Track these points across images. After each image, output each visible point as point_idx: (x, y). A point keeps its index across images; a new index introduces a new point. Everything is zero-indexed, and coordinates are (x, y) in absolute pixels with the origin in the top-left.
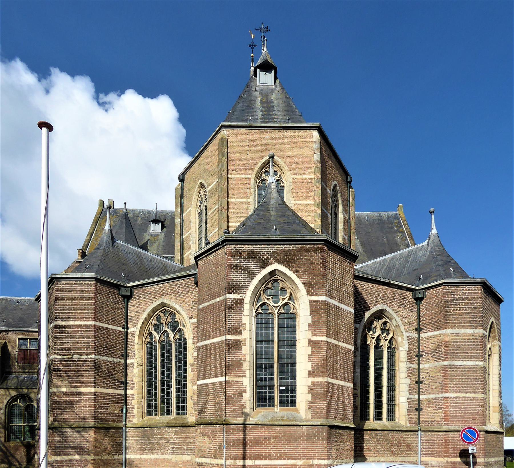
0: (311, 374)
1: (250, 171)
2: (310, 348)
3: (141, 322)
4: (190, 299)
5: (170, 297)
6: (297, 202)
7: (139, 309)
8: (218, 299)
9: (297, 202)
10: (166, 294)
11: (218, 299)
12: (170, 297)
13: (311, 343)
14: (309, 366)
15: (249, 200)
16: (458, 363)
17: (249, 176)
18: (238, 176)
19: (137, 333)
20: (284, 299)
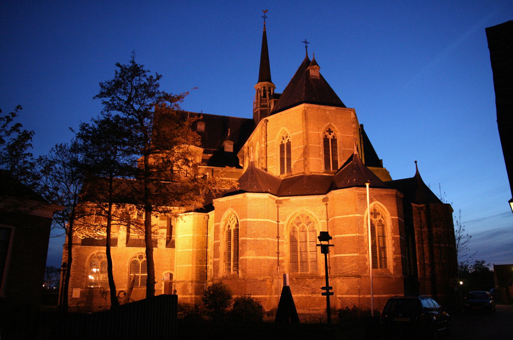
1: (320, 130)
3: (288, 219)
5: (307, 207)
6: (345, 149)
7: (287, 212)
8: (350, 216)
9: (345, 149)
10: (304, 205)
11: (350, 216)
12: (307, 207)
17: (320, 133)
19: (286, 225)
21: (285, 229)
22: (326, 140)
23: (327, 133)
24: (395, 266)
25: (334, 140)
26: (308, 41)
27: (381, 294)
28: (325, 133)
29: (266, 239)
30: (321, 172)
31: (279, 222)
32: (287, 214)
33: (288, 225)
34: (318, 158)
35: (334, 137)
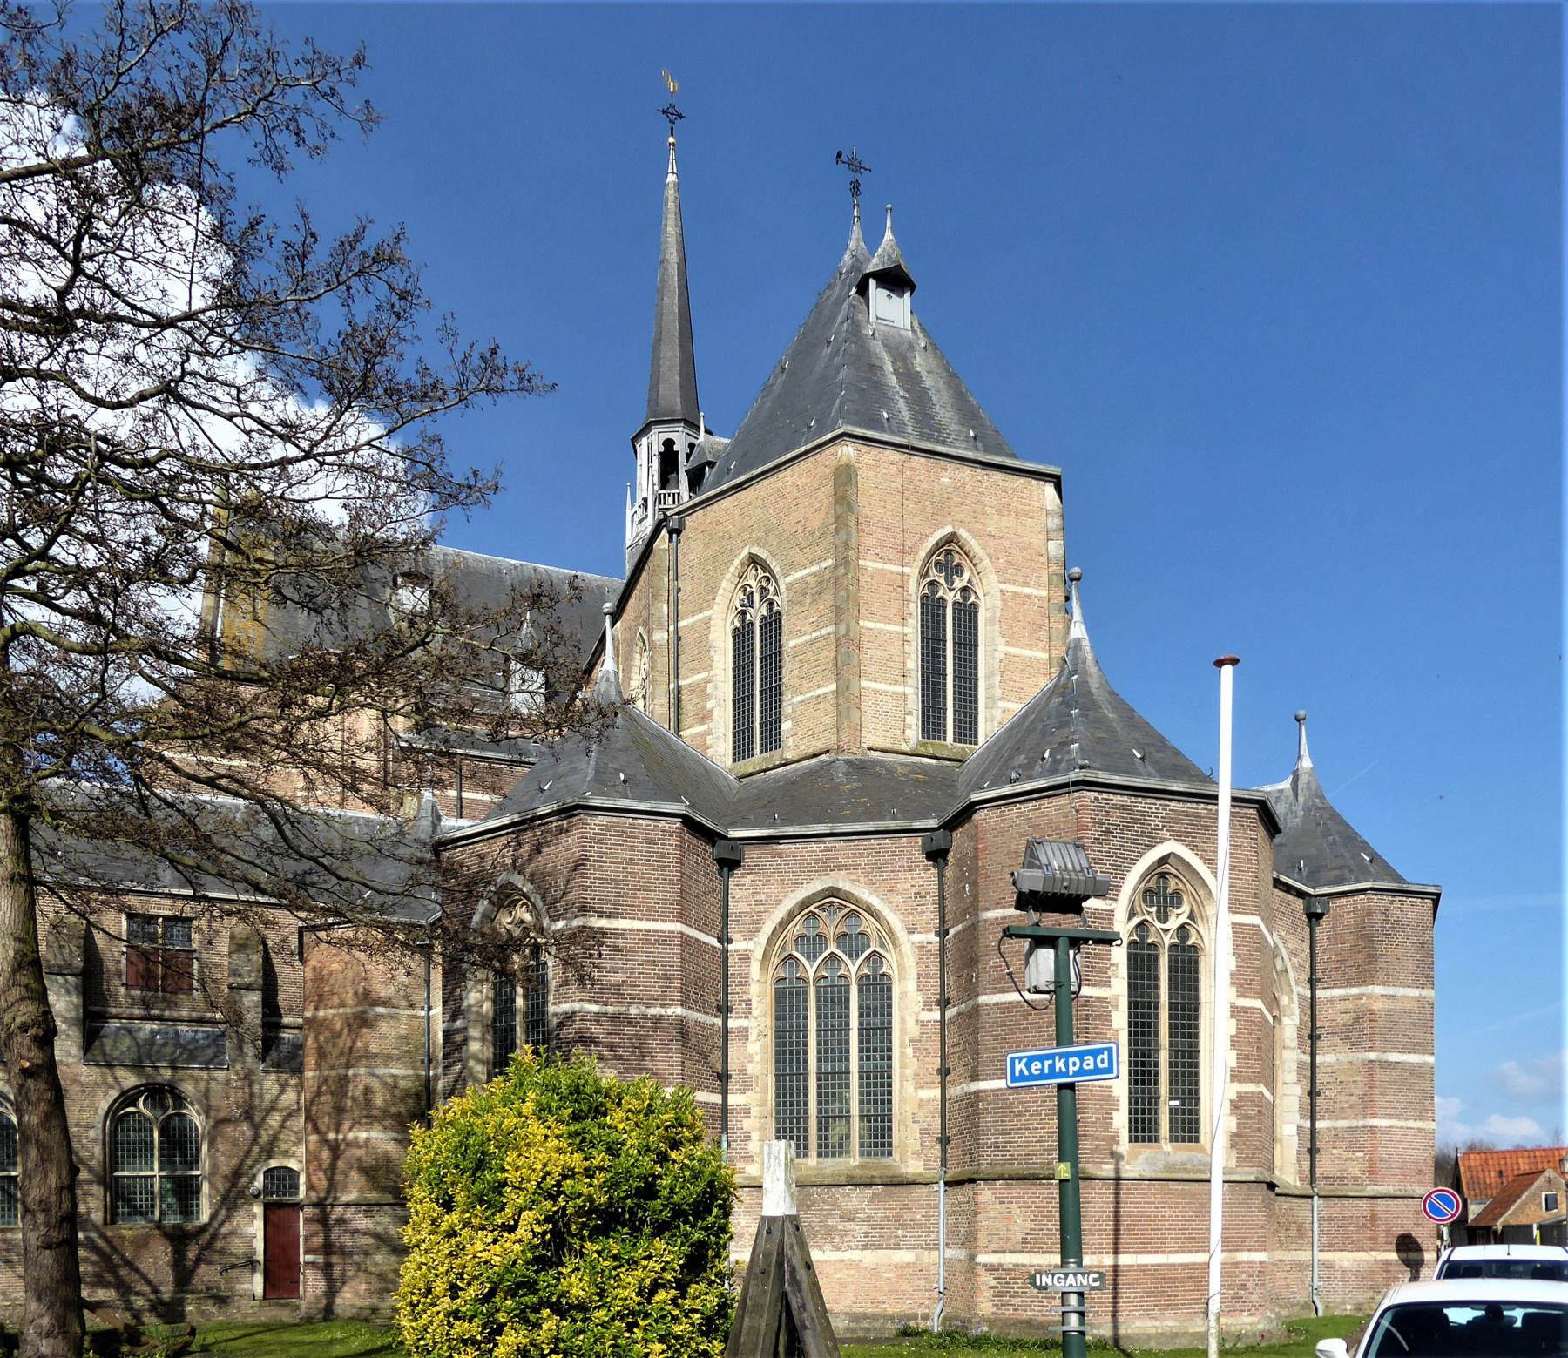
0: (1236, 1075)
2: (1234, 1021)
4: (908, 886)
7: (763, 897)
10: (840, 867)
13: (1236, 1012)
14: (1231, 1059)
15: (907, 630)
16: (1393, 1057)
18: (880, 566)
21: (755, 967)
22: (931, 608)
23: (934, 575)
25: (967, 614)
27: (1170, 1252)
30: (904, 747)
31: (730, 941)
32: (762, 908)
33: (766, 956)
34: (895, 683)
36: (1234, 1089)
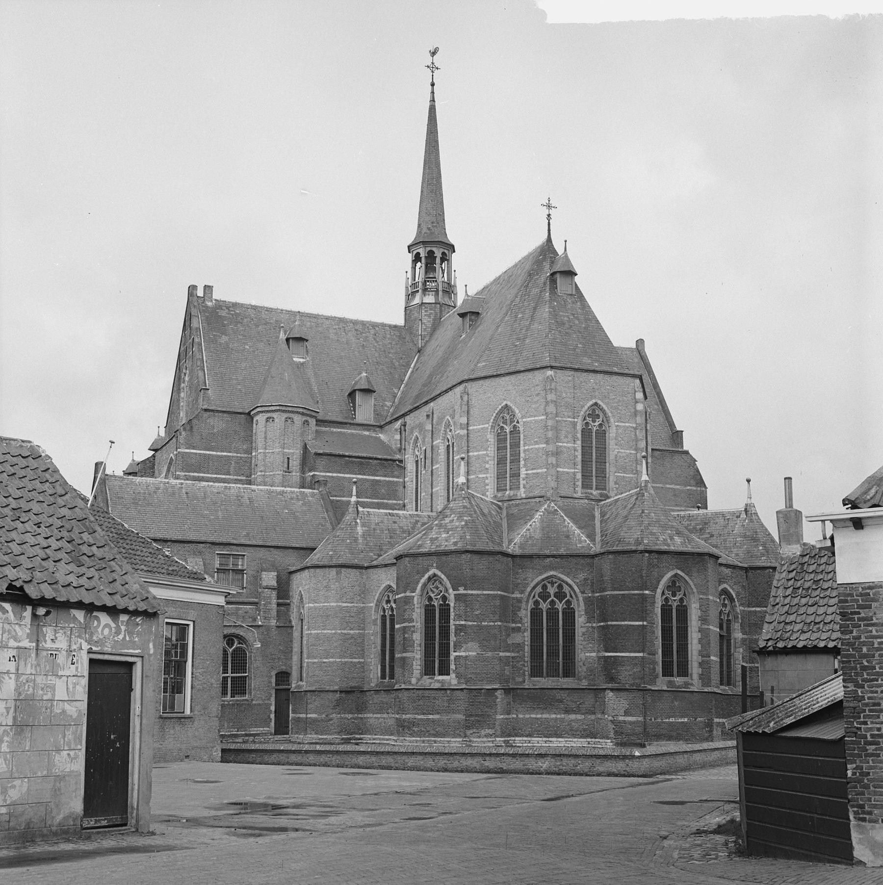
17: (576, 420)
20: (679, 595)
22: (586, 433)
23: (589, 420)
24: (700, 675)
26: (553, 203)
28: (585, 419)
29: (496, 624)
35: (681, 600)
36: (700, 659)
